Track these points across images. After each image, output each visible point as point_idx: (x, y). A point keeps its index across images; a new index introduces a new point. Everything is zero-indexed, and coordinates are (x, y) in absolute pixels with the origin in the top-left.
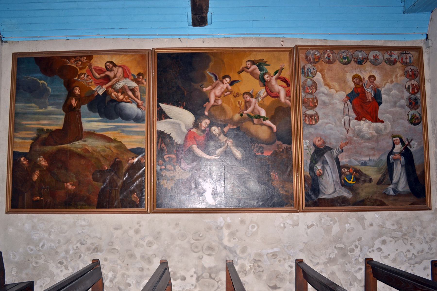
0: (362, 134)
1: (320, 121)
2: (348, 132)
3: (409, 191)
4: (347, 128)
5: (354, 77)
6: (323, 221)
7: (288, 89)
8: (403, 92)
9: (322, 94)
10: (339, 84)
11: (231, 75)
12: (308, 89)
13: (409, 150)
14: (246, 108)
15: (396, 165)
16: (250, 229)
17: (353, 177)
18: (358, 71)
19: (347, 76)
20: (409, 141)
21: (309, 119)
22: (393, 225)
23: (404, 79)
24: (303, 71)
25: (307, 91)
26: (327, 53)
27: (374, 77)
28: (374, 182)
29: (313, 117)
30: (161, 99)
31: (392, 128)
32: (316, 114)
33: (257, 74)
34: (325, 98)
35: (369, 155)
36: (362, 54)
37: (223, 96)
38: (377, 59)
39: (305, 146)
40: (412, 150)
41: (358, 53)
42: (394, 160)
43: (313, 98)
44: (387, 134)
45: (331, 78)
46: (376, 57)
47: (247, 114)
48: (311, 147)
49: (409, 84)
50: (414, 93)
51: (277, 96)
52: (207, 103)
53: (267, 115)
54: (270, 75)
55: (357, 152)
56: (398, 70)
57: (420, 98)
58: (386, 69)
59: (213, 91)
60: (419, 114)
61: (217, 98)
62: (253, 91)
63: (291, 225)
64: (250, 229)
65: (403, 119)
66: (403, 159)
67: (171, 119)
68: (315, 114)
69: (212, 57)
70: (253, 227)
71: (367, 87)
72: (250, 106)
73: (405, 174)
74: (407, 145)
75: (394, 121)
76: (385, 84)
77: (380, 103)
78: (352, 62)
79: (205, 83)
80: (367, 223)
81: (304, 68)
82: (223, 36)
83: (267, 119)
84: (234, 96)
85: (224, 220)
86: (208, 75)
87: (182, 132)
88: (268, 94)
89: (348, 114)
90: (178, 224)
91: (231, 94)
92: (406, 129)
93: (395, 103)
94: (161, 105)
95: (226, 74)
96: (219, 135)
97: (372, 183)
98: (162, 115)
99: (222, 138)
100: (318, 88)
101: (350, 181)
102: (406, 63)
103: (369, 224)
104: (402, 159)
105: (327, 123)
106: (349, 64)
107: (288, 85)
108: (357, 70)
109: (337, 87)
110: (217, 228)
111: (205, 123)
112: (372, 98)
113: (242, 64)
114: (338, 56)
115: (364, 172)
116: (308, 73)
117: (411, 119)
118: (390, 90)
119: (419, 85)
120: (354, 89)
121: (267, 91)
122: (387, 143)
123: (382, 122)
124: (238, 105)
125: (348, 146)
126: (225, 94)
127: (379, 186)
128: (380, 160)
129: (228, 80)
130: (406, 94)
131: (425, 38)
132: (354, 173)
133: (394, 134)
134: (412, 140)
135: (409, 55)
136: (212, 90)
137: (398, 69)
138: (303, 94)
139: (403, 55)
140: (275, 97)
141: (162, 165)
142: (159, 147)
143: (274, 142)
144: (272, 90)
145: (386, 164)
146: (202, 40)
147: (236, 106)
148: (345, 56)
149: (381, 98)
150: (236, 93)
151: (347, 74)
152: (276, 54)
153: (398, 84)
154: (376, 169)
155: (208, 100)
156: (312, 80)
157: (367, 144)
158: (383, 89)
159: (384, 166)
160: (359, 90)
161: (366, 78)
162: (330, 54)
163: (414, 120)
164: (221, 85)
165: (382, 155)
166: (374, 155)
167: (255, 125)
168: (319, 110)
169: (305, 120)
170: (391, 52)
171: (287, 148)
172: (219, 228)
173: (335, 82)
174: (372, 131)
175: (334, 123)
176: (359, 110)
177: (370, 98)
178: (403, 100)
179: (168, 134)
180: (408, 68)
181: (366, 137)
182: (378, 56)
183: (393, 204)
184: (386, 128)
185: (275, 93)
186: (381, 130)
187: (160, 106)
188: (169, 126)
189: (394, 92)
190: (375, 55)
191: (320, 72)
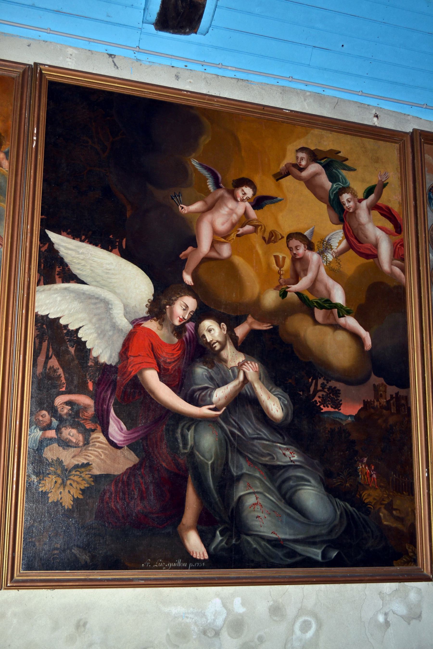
7: (398, 238)
11: (257, 179)
14: (296, 279)
16: (298, 632)
30: (55, 218)
33: (322, 187)
37: (233, 236)
47: (298, 293)
51: (371, 254)
52: (190, 249)
53: (347, 300)
54: (354, 195)
59: (208, 218)
61: (218, 238)
62: (312, 232)
63: (402, 617)
64: (298, 632)
67: (83, 283)
69: (206, 121)
70: (306, 627)
72: (305, 271)
79: (186, 192)
82: (231, 74)
83: (349, 313)
84: (264, 238)
85: (224, 605)
86: (196, 169)
87: (114, 326)
88: (350, 246)
90: (85, 624)
91: (255, 231)
94: (53, 236)
95: (244, 175)
96: (223, 346)
98: (54, 269)
99: (232, 357)
107: (398, 229)
110: (204, 632)
111: (183, 307)
113: (284, 156)
121: (346, 237)
124: (274, 265)
126: (241, 230)
129: (249, 191)
136: (203, 213)
140: (367, 256)
141: (49, 427)
142: (40, 369)
143: (366, 379)
144: (361, 235)
146: (174, 71)
147: (269, 266)
150: (269, 230)
152: (369, 143)
155: (193, 241)
164: (231, 204)
167: (318, 327)
171: (397, 397)
172: (211, 634)
179: (72, 327)
185: (365, 245)
187: (49, 240)
188: (76, 305)
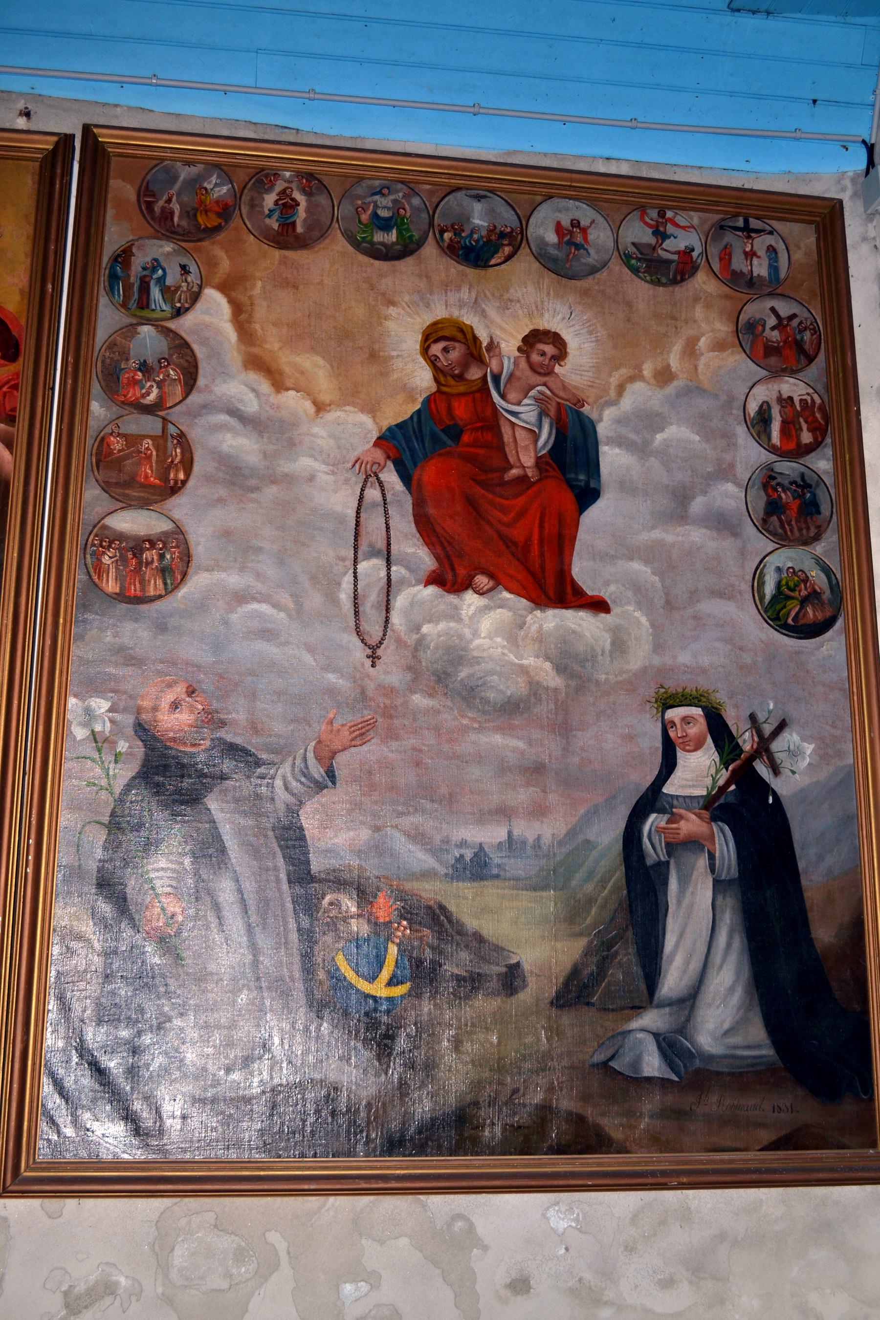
0: (463, 673)
1: (197, 583)
2: (374, 658)
3: (768, 1052)
4: (374, 631)
5: (431, 335)
6: (180, 1257)
8: (728, 436)
9: (223, 418)
10: (339, 366)
12: (134, 382)
13: (765, 788)
15: (684, 881)
17: (393, 950)
18: (462, 304)
19: (391, 325)
20: (767, 729)
21: (123, 559)
22: (668, 1283)
23: (738, 365)
24: (113, 278)
25: (132, 394)
26: (280, 186)
27: (556, 339)
28: (537, 990)
29: (150, 555)
31: (658, 647)
32: (177, 540)
34: (240, 444)
35: (504, 813)
36: (492, 212)
38: (578, 247)
39: (80, 733)
40: (783, 786)
41: (466, 201)
42: (671, 848)
43: (160, 440)
44: (630, 685)
45: (292, 325)
46: (572, 236)
48: (122, 746)
49: (762, 394)
50: (801, 451)
55: (427, 791)
56: (699, 312)
57: (829, 480)
58: (629, 305)
60: (827, 571)
65: (730, 598)
66: (724, 845)
68: (164, 537)
71: (512, 396)
73: (738, 943)
74: (752, 758)
75: (670, 604)
76: (621, 389)
77: (588, 495)
78: (430, 250)
80: (491, 1271)
81: (124, 257)
89: (381, 544)
92: (747, 659)
93: (682, 498)
97: (525, 996)
100: (201, 382)
101: (372, 978)
102: (751, 282)
103: (502, 1277)
104: (719, 839)
105: (241, 598)
106: (410, 261)
108: (453, 297)
109: (324, 382)
112: (540, 462)
114: (346, 210)
115: (471, 923)
116: (145, 289)
117: (774, 598)
118: (651, 421)
119: (822, 408)
120: (429, 401)
122: (623, 742)
123: (599, 606)
125: (371, 751)
127: (567, 1019)
128: (576, 846)
130: (750, 455)
131: (862, 165)
132: (403, 930)
133: (673, 685)
134: (782, 726)
135: (770, 240)
137: (704, 315)
138: (98, 409)
139: (729, 237)
145: (620, 873)
148: (384, 213)
149: (593, 466)
151: (392, 311)
153: (700, 390)
154: (549, 902)
156: (167, 332)
157: (498, 739)
158: (609, 414)
159: (604, 882)
160: (462, 411)
161: (510, 346)
162: (298, 196)
163: (793, 607)
165: (594, 812)
166: (539, 811)
168: (196, 513)
169: (99, 568)
170: (662, 214)
173: (313, 350)
174: (530, 661)
175: (285, 599)
176: (454, 527)
177: (528, 460)
178: (730, 487)
180: (758, 309)
181: (491, 695)
182: (584, 231)
183: (658, 1142)
184: (619, 646)
186: (591, 657)
189: (677, 433)
190: (566, 223)
191: (224, 288)
